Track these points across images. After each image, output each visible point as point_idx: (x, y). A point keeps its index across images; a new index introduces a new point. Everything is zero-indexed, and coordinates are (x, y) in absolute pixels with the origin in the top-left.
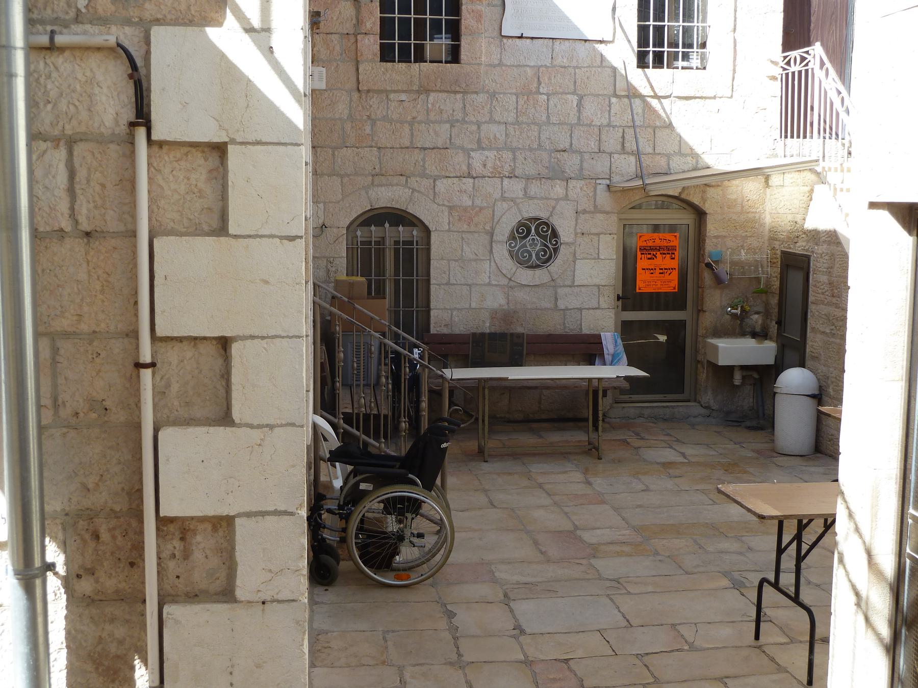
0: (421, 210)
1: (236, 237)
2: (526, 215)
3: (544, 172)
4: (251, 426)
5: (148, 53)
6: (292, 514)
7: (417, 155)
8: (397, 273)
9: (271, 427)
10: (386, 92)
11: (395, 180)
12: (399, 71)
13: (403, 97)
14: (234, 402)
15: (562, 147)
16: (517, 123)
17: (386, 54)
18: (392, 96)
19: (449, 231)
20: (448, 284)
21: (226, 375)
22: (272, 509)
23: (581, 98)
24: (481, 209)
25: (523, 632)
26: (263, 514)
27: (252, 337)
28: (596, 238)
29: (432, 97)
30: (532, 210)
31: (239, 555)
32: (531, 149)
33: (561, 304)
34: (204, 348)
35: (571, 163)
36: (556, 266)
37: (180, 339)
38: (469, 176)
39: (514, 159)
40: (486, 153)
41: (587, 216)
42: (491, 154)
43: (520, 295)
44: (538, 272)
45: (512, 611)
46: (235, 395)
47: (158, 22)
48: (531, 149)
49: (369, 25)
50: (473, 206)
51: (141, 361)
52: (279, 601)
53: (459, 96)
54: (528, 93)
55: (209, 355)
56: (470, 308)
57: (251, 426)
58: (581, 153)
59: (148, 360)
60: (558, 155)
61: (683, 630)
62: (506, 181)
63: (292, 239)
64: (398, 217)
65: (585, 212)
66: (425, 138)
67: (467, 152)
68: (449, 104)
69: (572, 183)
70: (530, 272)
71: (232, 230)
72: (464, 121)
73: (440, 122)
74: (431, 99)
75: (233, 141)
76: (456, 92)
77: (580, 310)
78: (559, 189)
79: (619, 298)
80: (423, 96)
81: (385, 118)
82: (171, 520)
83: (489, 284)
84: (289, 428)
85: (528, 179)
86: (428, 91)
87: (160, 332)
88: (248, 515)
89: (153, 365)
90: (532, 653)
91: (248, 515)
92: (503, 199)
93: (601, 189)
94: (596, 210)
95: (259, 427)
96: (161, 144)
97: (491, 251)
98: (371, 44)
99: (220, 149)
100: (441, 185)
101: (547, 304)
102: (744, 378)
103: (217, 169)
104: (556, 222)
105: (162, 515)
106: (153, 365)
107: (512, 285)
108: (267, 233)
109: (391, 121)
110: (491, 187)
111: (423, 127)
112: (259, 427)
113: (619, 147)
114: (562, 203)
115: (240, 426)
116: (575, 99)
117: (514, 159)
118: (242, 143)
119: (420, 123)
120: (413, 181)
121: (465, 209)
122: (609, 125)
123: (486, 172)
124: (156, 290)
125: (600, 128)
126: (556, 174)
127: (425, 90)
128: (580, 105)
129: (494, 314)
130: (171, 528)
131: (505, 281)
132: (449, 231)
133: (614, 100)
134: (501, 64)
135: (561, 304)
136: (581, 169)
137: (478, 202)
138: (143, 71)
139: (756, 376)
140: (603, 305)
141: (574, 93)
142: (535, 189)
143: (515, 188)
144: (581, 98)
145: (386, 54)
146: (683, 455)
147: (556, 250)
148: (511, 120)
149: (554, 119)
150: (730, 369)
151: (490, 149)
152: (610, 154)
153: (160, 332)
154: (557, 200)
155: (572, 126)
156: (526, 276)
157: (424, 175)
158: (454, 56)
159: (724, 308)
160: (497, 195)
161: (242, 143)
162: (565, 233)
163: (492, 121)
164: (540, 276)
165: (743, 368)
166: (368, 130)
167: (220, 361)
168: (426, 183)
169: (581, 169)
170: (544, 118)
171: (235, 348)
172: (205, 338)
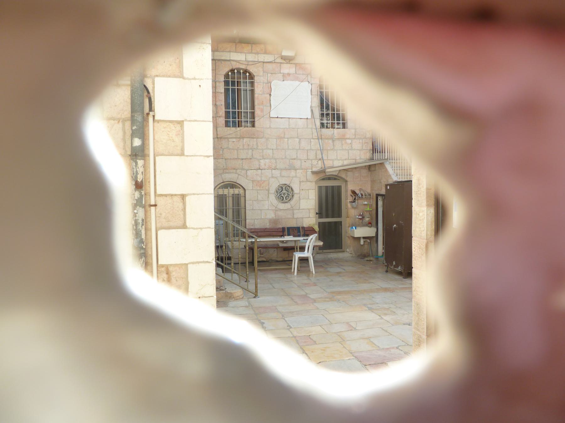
0: (242, 181)
1: (187, 156)
2: (281, 183)
3: (287, 167)
4: (194, 229)
5: (154, 88)
6: (209, 262)
7: (240, 162)
8: (233, 206)
9: (201, 229)
10: (228, 138)
11: (232, 171)
12: (232, 130)
13: (234, 140)
14: (187, 219)
15: (293, 158)
16: (277, 149)
17: (227, 124)
18: (230, 140)
19: (252, 189)
20: (253, 210)
21: (184, 209)
22: (202, 260)
23: (300, 139)
24: (264, 181)
25: (291, 327)
26: (199, 262)
27: (194, 194)
28: (307, 191)
29: (245, 140)
30: (283, 181)
31: (190, 279)
32: (282, 159)
33: (295, 216)
34: (175, 198)
35: (297, 164)
36: (293, 202)
37: (166, 195)
38: (259, 169)
39: (276, 162)
40: (266, 160)
41: (304, 183)
42: (267, 161)
43: (280, 213)
44: (286, 204)
45: (286, 321)
46: (187, 216)
47: (157, 76)
48: (282, 159)
49: (221, 114)
50: (261, 180)
51: (152, 204)
52: (205, 297)
53: (255, 139)
54: (280, 138)
55: (177, 201)
56: (261, 219)
57: (194, 229)
58: (300, 160)
59: (153, 203)
60: (292, 161)
61: (351, 323)
62: (273, 171)
63: (208, 157)
64: (233, 185)
65: (303, 182)
66: (243, 155)
67: (259, 160)
68: (253, 142)
69: (298, 171)
70: (283, 205)
71: (186, 153)
72: (257, 149)
73: (248, 149)
74: (244, 141)
75: (186, 120)
76: (254, 138)
77: (303, 218)
78: (293, 173)
79: (317, 214)
80: (242, 140)
81: (228, 148)
82: (163, 266)
83: (268, 209)
84: (209, 229)
85: (281, 170)
86: (243, 138)
87: (159, 192)
88: (193, 263)
89: (155, 205)
90: (295, 334)
91: (193, 263)
92: (273, 177)
93: (309, 173)
94: (307, 181)
95: (197, 229)
96: (158, 121)
97: (268, 197)
98: (222, 121)
99: (181, 123)
100: (249, 173)
101: (290, 216)
102: (364, 242)
103: (180, 131)
104: (292, 185)
105: (159, 263)
106: (155, 205)
107: (276, 210)
108: (199, 154)
109: (230, 149)
110: (268, 173)
111: (242, 151)
112: (197, 229)
113: (315, 157)
114: (294, 178)
115: (189, 228)
116: (297, 140)
117: (276, 162)
118: (189, 121)
119: (240, 149)
120: (238, 171)
121: (258, 181)
122: (311, 149)
123: (266, 168)
124: (157, 176)
125: (307, 150)
126: (292, 168)
127: (242, 137)
128: (299, 142)
129: (270, 221)
130: (163, 269)
131: (274, 208)
132: (252, 189)
133: (312, 140)
134: (270, 127)
135: (295, 216)
136: (301, 165)
137: (263, 179)
138: (152, 94)
139: (369, 241)
140: (311, 216)
141: (297, 138)
142: (284, 173)
143: (276, 173)
144: (300, 139)
145: (227, 124)
146: (344, 269)
147: (293, 196)
148: (275, 148)
149: (290, 148)
150: (359, 238)
151: (267, 159)
152: (312, 160)
153: (159, 192)
154: (293, 177)
155: (297, 150)
156: (282, 206)
157: (243, 169)
158: (253, 126)
159: (355, 216)
160: (270, 176)
161: (189, 121)
162: (296, 190)
163: (267, 149)
164: (287, 206)
165: (364, 238)
166: (221, 152)
167: (181, 204)
168: (244, 172)
169: (301, 165)
170: (287, 147)
171: (187, 199)
172: (176, 195)
